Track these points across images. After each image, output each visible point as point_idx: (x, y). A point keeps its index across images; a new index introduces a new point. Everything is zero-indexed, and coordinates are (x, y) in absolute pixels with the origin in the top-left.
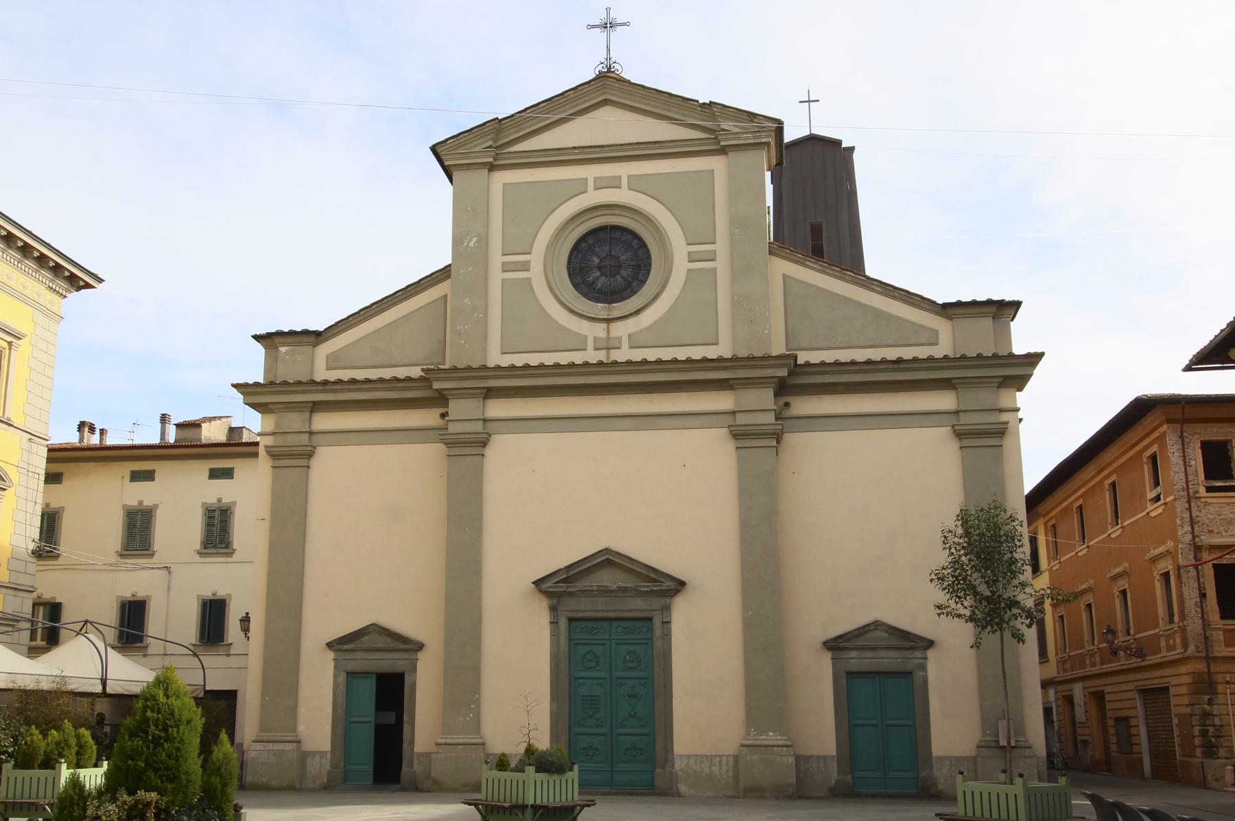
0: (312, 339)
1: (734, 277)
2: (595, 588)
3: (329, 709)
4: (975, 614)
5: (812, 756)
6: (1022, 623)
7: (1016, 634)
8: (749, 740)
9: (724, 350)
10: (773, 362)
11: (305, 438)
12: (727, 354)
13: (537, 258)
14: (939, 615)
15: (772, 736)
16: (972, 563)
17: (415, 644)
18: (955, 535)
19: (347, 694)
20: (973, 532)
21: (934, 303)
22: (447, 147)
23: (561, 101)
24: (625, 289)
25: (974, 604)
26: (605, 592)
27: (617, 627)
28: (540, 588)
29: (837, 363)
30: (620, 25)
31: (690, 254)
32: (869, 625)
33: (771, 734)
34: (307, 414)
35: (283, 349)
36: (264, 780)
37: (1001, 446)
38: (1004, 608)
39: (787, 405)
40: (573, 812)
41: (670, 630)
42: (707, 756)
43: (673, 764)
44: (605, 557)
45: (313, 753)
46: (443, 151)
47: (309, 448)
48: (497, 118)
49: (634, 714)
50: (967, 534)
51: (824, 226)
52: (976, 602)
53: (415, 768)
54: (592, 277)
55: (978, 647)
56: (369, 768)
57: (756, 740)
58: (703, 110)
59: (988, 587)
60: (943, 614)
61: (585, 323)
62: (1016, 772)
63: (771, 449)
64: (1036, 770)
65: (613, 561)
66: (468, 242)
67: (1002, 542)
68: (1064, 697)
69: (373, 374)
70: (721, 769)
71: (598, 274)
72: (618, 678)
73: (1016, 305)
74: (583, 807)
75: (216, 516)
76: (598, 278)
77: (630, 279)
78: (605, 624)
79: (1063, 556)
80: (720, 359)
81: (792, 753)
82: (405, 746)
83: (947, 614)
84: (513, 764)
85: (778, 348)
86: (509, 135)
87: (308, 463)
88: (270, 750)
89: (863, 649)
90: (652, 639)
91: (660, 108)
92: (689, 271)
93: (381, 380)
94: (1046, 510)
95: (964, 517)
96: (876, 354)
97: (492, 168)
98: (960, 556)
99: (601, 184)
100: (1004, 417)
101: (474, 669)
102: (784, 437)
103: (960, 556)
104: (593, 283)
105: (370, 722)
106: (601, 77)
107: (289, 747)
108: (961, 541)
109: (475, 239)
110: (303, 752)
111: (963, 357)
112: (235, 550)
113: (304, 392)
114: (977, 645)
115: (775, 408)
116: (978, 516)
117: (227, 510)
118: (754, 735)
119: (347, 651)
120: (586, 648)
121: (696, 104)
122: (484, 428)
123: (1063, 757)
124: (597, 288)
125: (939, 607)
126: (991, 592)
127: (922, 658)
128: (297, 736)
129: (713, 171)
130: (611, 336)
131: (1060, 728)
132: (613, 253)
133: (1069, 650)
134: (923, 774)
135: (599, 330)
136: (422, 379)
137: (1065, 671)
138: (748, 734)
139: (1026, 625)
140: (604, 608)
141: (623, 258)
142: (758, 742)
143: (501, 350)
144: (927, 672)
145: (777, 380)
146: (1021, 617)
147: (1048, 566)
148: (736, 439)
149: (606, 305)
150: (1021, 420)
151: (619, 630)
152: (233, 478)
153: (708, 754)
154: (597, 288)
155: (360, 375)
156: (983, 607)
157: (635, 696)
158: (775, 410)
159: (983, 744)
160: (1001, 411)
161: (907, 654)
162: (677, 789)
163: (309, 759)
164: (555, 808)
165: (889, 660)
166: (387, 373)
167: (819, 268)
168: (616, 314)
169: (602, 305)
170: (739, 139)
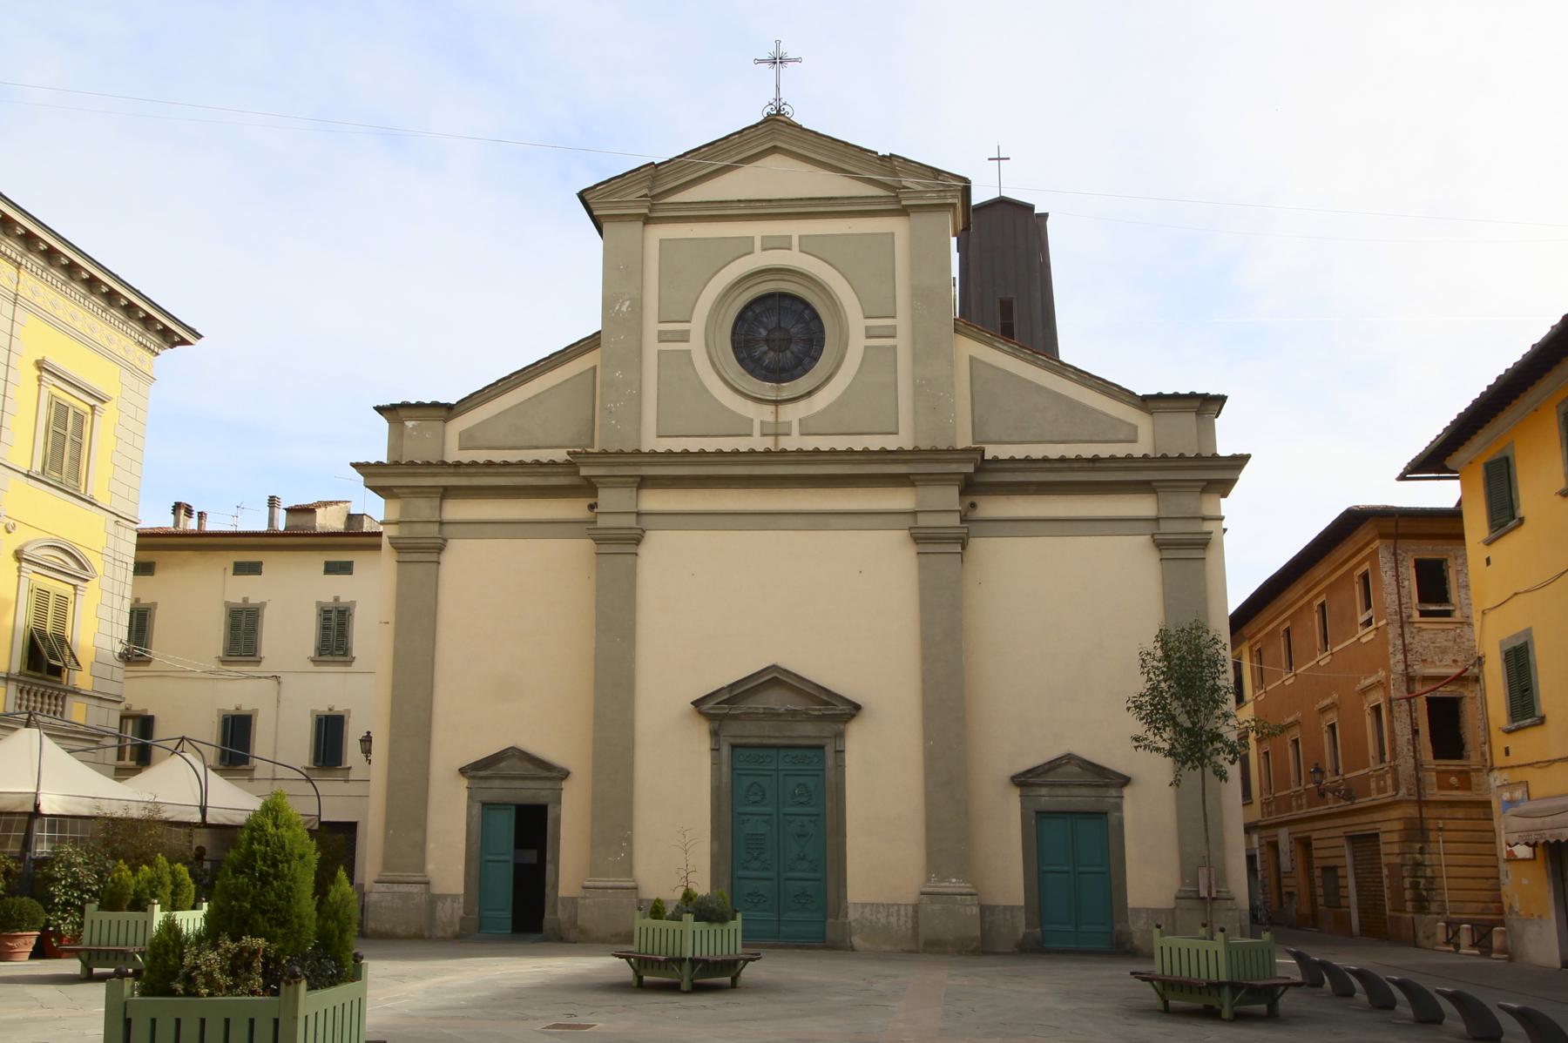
0: (443, 413)
1: (916, 358)
2: (761, 711)
3: (462, 846)
5: (998, 906)
6: (1225, 759)
9: (903, 440)
10: (956, 456)
11: (434, 529)
12: (908, 446)
14: (1136, 748)
21: (1133, 394)
23: (725, 146)
25: (1174, 737)
26: (772, 715)
29: (1028, 460)
30: (791, 60)
31: (867, 328)
33: (954, 880)
34: (436, 502)
35: (409, 424)
36: (388, 927)
38: (1205, 742)
39: (973, 505)
42: (883, 905)
45: (444, 897)
46: (592, 198)
47: (440, 541)
48: (653, 163)
53: (559, 915)
55: (1178, 785)
56: (507, 914)
59: (1189, 718)
62: (1217, 926)
64: (1238, 925)
67: (1204, 668)
69: (513, 456)
70: (899, 919)
71: (765, 348)
72: (785, 814)
73: (1221, 400)
74: (747, 961)
75: (333, 618)
76: (765, 353)
78: (773, 752)
80: (900, 451)
82: (548, 890)
84: (669, 912)
85: (964, 441)
86: (667, 183)
87: (439, 558)
89: (1053, 785)
90: (823, 770)
93: (521, 464)
95: (1163, 638)
97: (647, 220)
98: (1159, 682)
99: (770, 244)
100: (1208, 526)
102: (970, 543)
103: (1159, 682)
104: (760, 358)
106: (769, 119)
108: (1160, 665)
109: (628, 303)
110: (434, 895)
111: (1164, 457)
113: (434, 475)
114: (1176, 783)
115: (960, 508)
119: (482, 778)
121: (875, 156)
125: (1136, 739)
128: (426, 876)
129: (893, 234)
130: (780, 420)
131: (1264, 878)
132: (782, 325)
134: (1118, 927)
135: (767, 412)
136: (567, 464)
137: (1270, 814)
138: (929, 880)
139: (1229, 761)
141: (794, 330)
142: (940, 890)
145: (962, 477)
146: (1224, 753)
149: (774, 384)
150: (1225, 530)
155: (497, 456)
158: (960, 511)
159: (1182, 895)
160: (1204, 519)
161: (1101, 791)
162: (851, 942)
163: (439, 903)
164: (716, 963)
165: (1081, 798)
166: (529, 456)
168: (785, 395)
169: (770, 384)
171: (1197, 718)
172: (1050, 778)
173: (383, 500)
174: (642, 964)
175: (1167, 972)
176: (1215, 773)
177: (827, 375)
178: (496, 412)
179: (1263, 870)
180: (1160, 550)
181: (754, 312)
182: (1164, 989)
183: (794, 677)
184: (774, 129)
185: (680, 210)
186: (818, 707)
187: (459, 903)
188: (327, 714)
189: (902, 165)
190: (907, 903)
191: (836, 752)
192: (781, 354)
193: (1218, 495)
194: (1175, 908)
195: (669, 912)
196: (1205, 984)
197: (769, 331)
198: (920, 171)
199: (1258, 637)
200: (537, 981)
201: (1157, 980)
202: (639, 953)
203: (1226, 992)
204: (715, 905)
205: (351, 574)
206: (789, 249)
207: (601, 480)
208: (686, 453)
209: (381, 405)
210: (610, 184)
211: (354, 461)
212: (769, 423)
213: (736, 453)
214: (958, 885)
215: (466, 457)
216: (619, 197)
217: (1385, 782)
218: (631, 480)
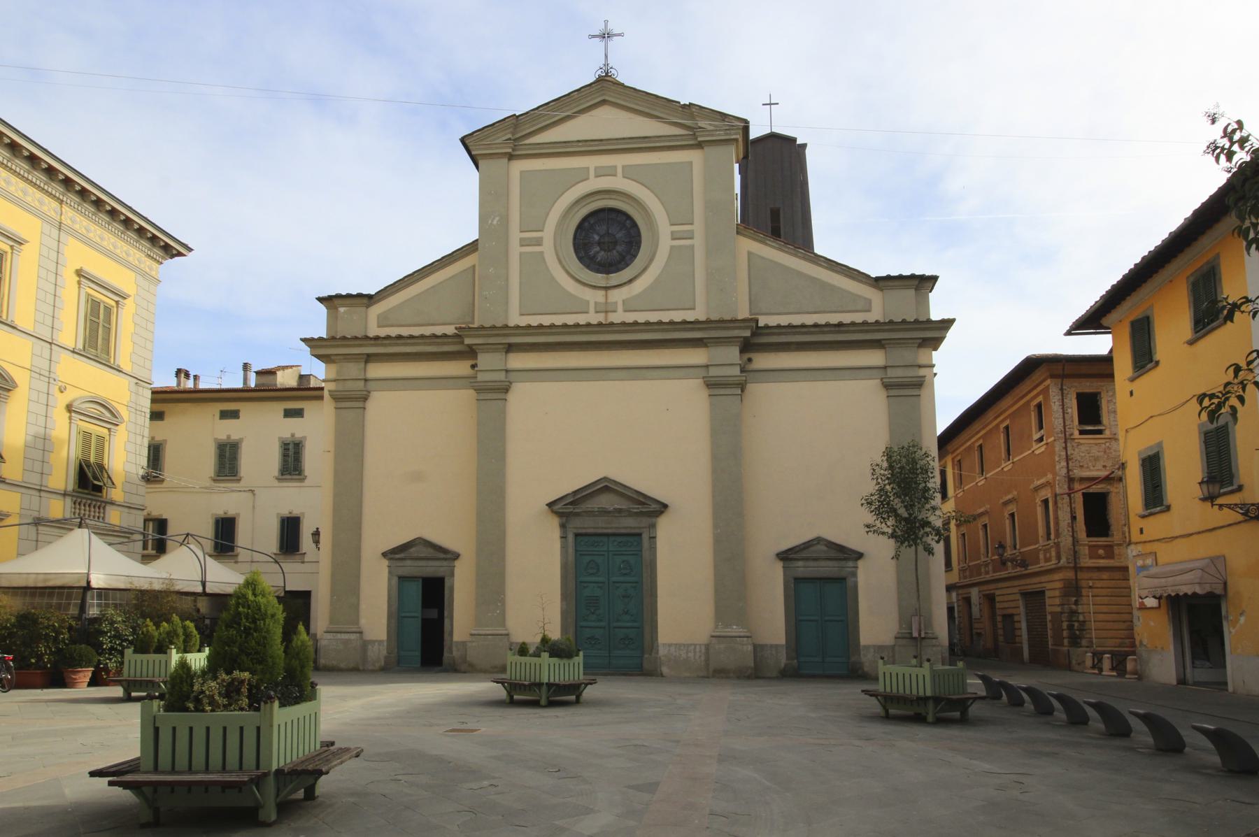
0: (365, 301)
3: (385, 607)
5: (766, 645)
8: (717, 632)
9: (698, 314)
12: (702, 318)
13: (548, 234)
14: (867, 532)
16: (894, 491)
21: (868, 276)
25: (896, 524)
26: (604, 512)
29: (790, 326)
31: (672, 233)
33: (735, 627)
34: (362, 365)
35: (342, 310)
36: (335, 663)
37: (919, 395)
39: (750, 360)
41: (655, 543)
42: (684, 645)
45: (374, 642)
47: (365, 393)
50: (891, 467)
56: (417, 654)
61: (587, 290)
64: (940, 657)
66: (492, 221)
69: (416, 331)
71: (598, 249)
73: (934, 279)
74: (587, 685)
76: (598, 252)
78: (605, 539)
80: (697, 322)
82: (446, 636)
83: (874, 531)
84: (531, 651)
85: (743, 313)
87: (364, 405)
88: (339, 639)
89: (807, 559)
90: (641, 551)
93: (422, 337)
95: (889, 454)
97: (511, 157)
98: (885, 485)
99: (601, 173)
100: (922, 372)
103: (885, 485)
104: (594, 257)
105: (417, 617)
106: (600, 80)
107: (353, 637)
108: (886, 473)
109: (497, 218)
111: (891, 322)
113: (361, 346)
114: (896, 557)
115: (740, 362)
116: (900, 453)
122: (506, 378)
125: (868, 526)
128: (360, 628)
130: (609, 301)
131: (960, 623)
134: (853, 659)
135: (599, 296)
136: (456, 336)
138: (716, 627)
140: (604, 526)
149: (605, 275)
150: (935, 374)
151: (615, 543)
155: (405, 332)
157: (629, 597)
158: (740, 364)
159: (900, 635)
160: (920, 366)
161: (843, 563)
163: (370, 647)
164: (565, 686)
165: (827, 568)
166: (428, 331)
170: (712, 135)
174: (512, 687)
175: (888, 690)
180: (887, 389)
191: (650, 538)
193: (931, 349)
194: (895, 645)
195: (531, 651)
197: (601, 236)
199: (958, 451)
203: (931, 705)
206: (615, 175)
208: (541, 326)
209: (321, 296)
213: (577, 325)
216: (490, 141)
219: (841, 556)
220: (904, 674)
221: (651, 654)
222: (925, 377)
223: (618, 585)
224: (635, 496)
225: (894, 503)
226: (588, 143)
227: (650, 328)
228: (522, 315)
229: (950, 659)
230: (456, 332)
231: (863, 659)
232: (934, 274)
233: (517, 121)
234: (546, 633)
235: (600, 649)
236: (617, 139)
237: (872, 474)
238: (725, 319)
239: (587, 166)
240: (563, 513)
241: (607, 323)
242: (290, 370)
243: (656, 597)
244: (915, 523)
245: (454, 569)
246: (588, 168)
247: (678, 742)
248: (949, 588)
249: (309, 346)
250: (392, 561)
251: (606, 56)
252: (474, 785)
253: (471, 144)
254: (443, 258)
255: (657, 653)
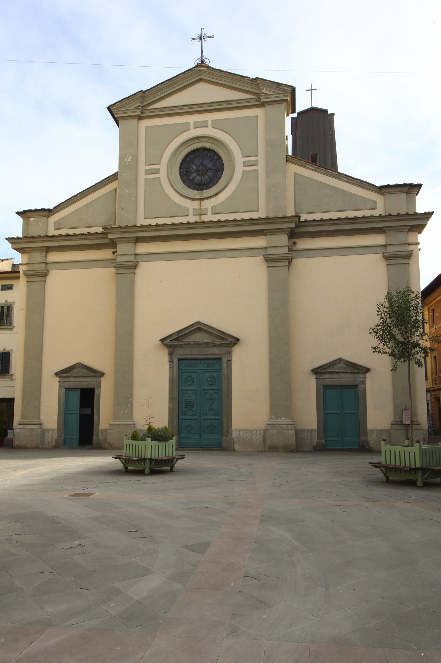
0: (47, 213)
1: (268, 174)
2: (192, 343)
3: (56, 407)
4: (395, 352)
5: (304, 430)
6: (421, 356)
7: (417, 362)
8: (271, 421)
9: (261, 214)
10: (287, 220)
11: (43, 266)
12: (263, 216)
13: (163, 167)
14: (374, 352)
15: (283, 419)
16: (394, 323)
17: (99, 373)
18: (384, 307)
19: (65, 400)
20: (395, 305)
21: (374, 186)
22: (116, 107)
23: (176, 80)
24: (209, 183)
25: (394, 346)
26: (197, 345)
27: (203, 363)
28: (164, 343)
29: (322, 220)
30: (208, 37)
31: (244, 162)
32: (336, 360)
33: (283, 418)
34: (44, 254)
35: (32, 219)
36: (24, 444)
37: (409, 263)
38: (411, 348)
39: (295, 243)
40: (172, 462)
41: (231, 364)
42: (249, 430)
43: (232, 434)
44: (198, 326)
45: (49, 430)
46: (114, 109)
47: (46, 271)
48: (142, 91)
49: (212, 408)
50: (391, 306)
51: (318, 156)
52: (395, 345)
53: (100, 437)
54: (192, 176)
55: (395, 370)
56: (77, 437)
57: (274, 421)
58: (253, 82)
59: (402, 336)
60: (376, 352)
61: (188, 201)
62: (415, 439)
63: (286, 267)
64: (422, 437)
65: (201, 328)
66: (127, 159)
67: (411, 311)
68: (435, 397)
69: (78, 231)
70: (256, 437)
71: (196, 174)
72: (204, 390)
73: (419, 186)
74: (178, 459)
75: (5, 309)
76: (195, 177)
77: (212, 177)
78: (198, 362)
79: (437, 326)
80: (260, 219)
81: (294, 428)
82: (95, 426)
83: (379, 352)
84: (140, 438)
85: (291, 212)
86: (149, 100)
87: (45, 279)
88: (27, 428)
89: (332, 373)
90: (221, 369)
91: (229, 82)
92: (244, 171)
93: (82, 234)
94: (429, 302)
95: (389, 297)
96: (342, 215)
97: (140, 118)
98: (387, 319)
99: (198, 125)
100: (411, 248)
101: (130, 387)
102: (292, 261)
103: (387, 319)
104: (193, 179)
105: (77, 414)
106: (198, 66)
107: (36, 427)
108: (388, 310)
109: (130, 157)
110: (44, 429)
111: (390, 215)
112: (14, 326)
113: (43, 242)
114: (394, 369)
115: (288, 245)
116: (398, 296)
117: (10, 306)
118: (274, 419)
119: (65, 377)
120: (188, 374)
121: (248, 79)
122: (135, 259)
123: (434, 428)
124: (195, 183)
125: (374, 348)
126: (404, 339)
127: (364, 378)
128: (40, 421)
129: (257, 116)
130: (202, 208)
131: (432, 413)
132: (203, 163)
133: (439, 373)
134: (362, 439)
135: (196, 205)
136: (103, 233)
137: (436, 384)
138: (271, 418)
139: (423, 357)
140: (197, 353)
141: (209, 165)
142: (276, 423)
143: (144, 217)
144: (366, 385)
145: (289, 230)
146: (421, 353)
147: (429, 330)
148: (267, 262)
149: (200, 191)
150: (420, 249)
151: (205, 365)
152: (13, 290)
153: (249, 429)
154: (195, 183)
155: (71, 232)
156: (399, 348)
157: (213, 399)
158: (288, 246)
159: (394, 423)
160: (409, 244)
161: (356, 376)
162: (234, 447)
163: (46, 433)
164: (161, 460)
165: (346, 379)
166: (85, 231)
167: (313, 169)
168: (205, 196)
169: (198, 191)
170: (271, 98)
171: (407, 336)
172: (330, 370)
173: (21, 254)
174: (127, 461)
175: (388, 463)
176: (416, 363)
177: (225, 185)
178: (70, 212)
179: (432, 410)
180: (387, 260)
181: (190, 158)
182: (386, 471)
183: (208, 327)
184: (200, 74)
185: (155, 112)
186: (219, 340)
187: (55, 433)
188: (3, 351)
189: (262, 83)
190: (260, 429)
191: (228, 360)
192: (203, 177)
193: (417, 233)
194: (391, 429)
195: (140, 438)
196: (408, 469)
197: (198, 167)
198: (270, 85)
199: (432, 303)
200: (77, 470)
201: (384, 467)
202: (126, 456)
203: (420, 473)
204: (162, 434)
205: (13, 290)
206: (207, 127)
207: (118, 240)
208: (157, 225)
209: (19, 211)
210: (122, 102)
211: (7, 237)
212: (196, 209)
213: (181, 224)
214: (285, 420)
215: (57, 233)
216: (127, 108)
217: (437, 382)
218: (132, 239)
219: (355, 370)
220: (400, 452)
221: (227, 436)
222: (413, 251)
223: (206, 392)
224: (217, 334)
225: (393, 332)
226: (189, 107)
227: (228, 224)
228: (145, 218)
229: (428, 437)
230: (103, 230)
231: (370, 439)
232: (419, 183)
233: (144, 94)
234: (151, 424)
235: (194, 434)
236: (208, 103)
237: (378, 311)
238: (278, 216)
239: (189, 122)
240: (170, 345)
241: (201, 222)
242: (7, 261)
243: (231, 399)
244: (409, 345)
245: (100, 384)
246: (189, 123)
247: (233, 503)
248: (428, 391)
249: (11, 244)
250: (61, 378)
251: (202, 51)
252: (66, 545)
253: (114, 110)
254: (96, 184)
255: (232, 436)
